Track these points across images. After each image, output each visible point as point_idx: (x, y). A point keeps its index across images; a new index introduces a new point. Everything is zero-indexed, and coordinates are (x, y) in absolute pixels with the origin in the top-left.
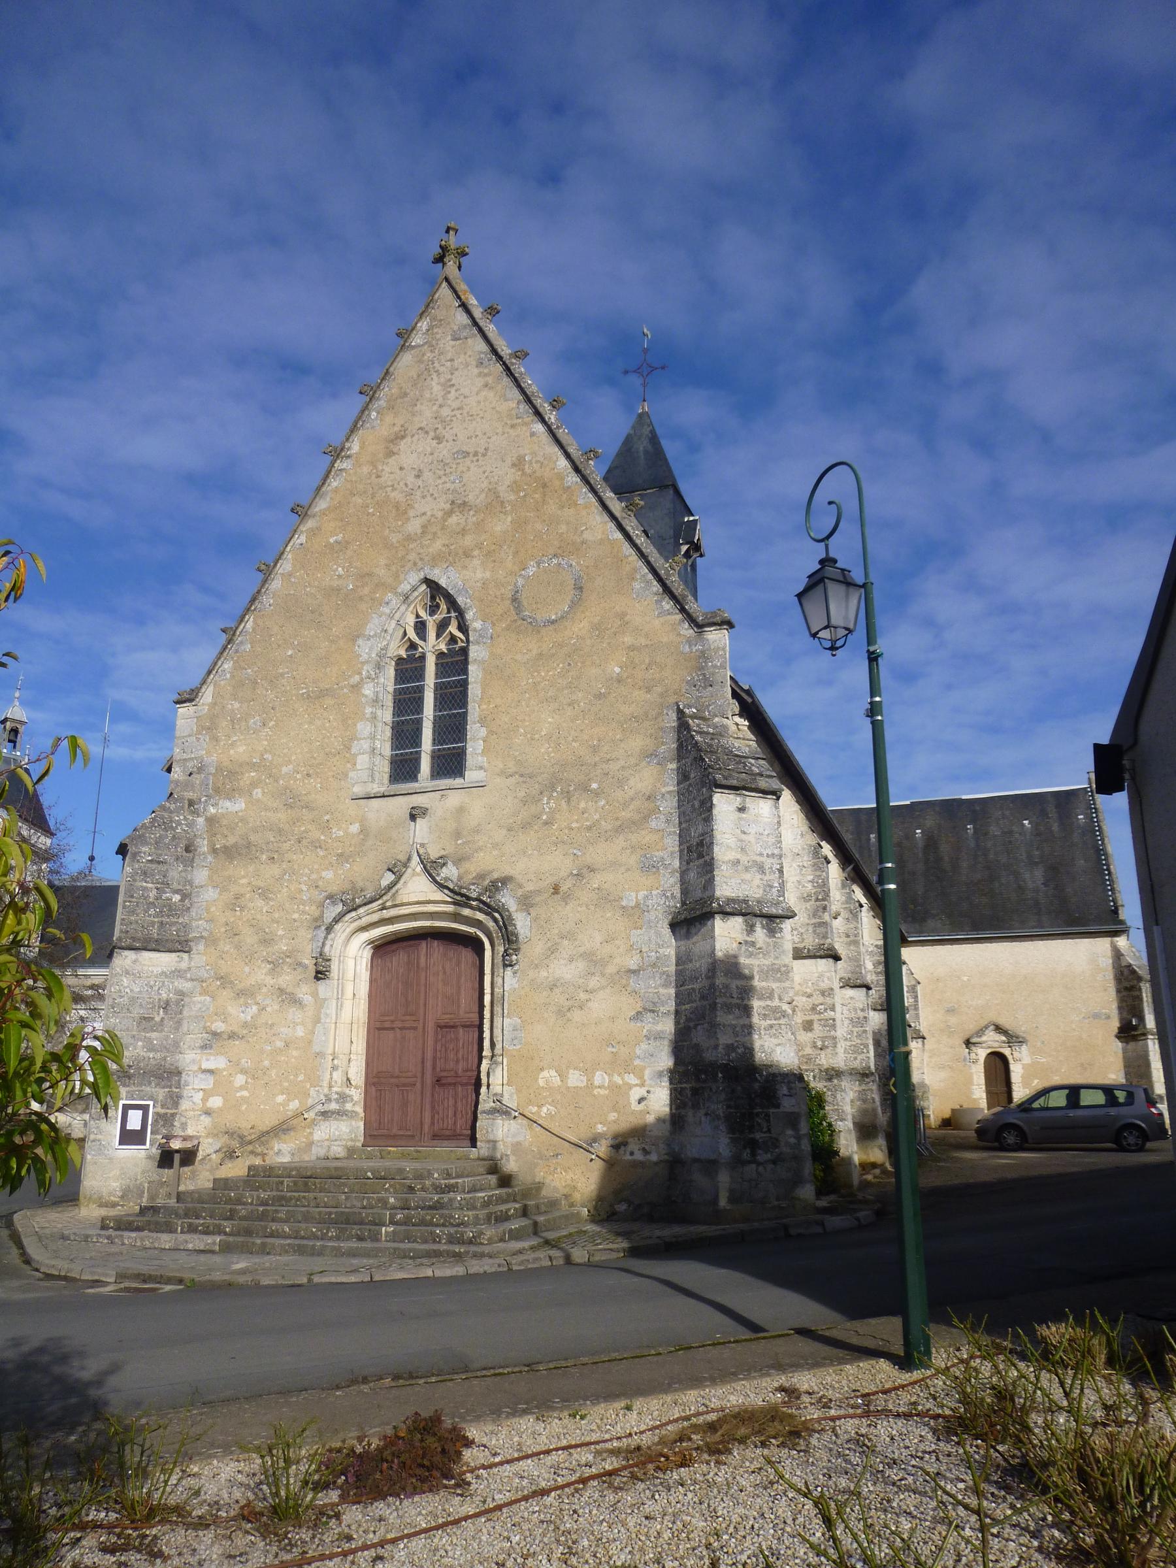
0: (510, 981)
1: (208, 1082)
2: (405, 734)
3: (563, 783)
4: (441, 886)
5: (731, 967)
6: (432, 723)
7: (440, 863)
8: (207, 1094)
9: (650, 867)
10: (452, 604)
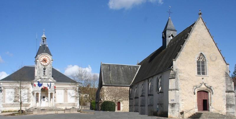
0: (212, 96)
1: (183, 105)
2: (199, 69)
3: (215, 78)
4: (206, 86)
5: (47, 47)
6: (201, 68)
7: (205, 84)
8: (183, 106)
9: (224, 87)
10: (203, 55)
